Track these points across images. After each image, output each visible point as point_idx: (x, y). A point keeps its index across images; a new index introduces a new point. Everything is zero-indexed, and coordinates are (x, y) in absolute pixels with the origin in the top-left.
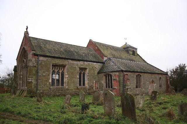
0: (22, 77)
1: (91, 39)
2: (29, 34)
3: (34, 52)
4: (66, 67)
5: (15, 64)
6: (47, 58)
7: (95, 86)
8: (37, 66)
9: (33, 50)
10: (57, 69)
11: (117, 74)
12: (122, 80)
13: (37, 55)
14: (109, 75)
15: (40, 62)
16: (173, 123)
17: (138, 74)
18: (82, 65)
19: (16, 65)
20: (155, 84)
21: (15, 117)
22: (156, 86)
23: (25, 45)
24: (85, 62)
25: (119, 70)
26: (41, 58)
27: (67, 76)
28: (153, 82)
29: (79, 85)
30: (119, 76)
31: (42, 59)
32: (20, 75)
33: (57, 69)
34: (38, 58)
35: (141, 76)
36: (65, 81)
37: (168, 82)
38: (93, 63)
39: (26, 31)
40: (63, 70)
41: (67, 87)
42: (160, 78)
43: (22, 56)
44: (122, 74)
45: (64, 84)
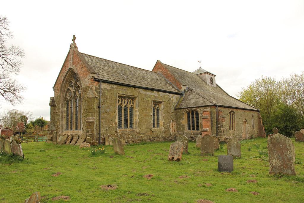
0: (65, 114)
1: (8, 20)
2: (77, 48)
3: (94, 75)
4: (137, 99)
5: (52, 94)
6: (112, 86)
8: (98, 98)
9: (92, 73)
11: (209, 109)
12: (216, 119)
13: (98, 81)
15: (102, 92)
17: (231, 110)
19: (53, 96)
20: (248, 125)
21: (98, 164)
22: (248, 126)
23: (73, 63)
24: (160, 93)
25: (211, 104)
26: (104, 86)
27: (138, 113)
28: (245, 121)
29: (152, 126)
32: (62, 112)
34: (100, 86)
35: (234, 112)
36: (134, 120)
37: (261, 121)
38: (169, 94)
40: (132, 103)
41: (138, 130)
42: (253, 115)
43: (67, 81)
44: (215, 110)
45: (134, 125)
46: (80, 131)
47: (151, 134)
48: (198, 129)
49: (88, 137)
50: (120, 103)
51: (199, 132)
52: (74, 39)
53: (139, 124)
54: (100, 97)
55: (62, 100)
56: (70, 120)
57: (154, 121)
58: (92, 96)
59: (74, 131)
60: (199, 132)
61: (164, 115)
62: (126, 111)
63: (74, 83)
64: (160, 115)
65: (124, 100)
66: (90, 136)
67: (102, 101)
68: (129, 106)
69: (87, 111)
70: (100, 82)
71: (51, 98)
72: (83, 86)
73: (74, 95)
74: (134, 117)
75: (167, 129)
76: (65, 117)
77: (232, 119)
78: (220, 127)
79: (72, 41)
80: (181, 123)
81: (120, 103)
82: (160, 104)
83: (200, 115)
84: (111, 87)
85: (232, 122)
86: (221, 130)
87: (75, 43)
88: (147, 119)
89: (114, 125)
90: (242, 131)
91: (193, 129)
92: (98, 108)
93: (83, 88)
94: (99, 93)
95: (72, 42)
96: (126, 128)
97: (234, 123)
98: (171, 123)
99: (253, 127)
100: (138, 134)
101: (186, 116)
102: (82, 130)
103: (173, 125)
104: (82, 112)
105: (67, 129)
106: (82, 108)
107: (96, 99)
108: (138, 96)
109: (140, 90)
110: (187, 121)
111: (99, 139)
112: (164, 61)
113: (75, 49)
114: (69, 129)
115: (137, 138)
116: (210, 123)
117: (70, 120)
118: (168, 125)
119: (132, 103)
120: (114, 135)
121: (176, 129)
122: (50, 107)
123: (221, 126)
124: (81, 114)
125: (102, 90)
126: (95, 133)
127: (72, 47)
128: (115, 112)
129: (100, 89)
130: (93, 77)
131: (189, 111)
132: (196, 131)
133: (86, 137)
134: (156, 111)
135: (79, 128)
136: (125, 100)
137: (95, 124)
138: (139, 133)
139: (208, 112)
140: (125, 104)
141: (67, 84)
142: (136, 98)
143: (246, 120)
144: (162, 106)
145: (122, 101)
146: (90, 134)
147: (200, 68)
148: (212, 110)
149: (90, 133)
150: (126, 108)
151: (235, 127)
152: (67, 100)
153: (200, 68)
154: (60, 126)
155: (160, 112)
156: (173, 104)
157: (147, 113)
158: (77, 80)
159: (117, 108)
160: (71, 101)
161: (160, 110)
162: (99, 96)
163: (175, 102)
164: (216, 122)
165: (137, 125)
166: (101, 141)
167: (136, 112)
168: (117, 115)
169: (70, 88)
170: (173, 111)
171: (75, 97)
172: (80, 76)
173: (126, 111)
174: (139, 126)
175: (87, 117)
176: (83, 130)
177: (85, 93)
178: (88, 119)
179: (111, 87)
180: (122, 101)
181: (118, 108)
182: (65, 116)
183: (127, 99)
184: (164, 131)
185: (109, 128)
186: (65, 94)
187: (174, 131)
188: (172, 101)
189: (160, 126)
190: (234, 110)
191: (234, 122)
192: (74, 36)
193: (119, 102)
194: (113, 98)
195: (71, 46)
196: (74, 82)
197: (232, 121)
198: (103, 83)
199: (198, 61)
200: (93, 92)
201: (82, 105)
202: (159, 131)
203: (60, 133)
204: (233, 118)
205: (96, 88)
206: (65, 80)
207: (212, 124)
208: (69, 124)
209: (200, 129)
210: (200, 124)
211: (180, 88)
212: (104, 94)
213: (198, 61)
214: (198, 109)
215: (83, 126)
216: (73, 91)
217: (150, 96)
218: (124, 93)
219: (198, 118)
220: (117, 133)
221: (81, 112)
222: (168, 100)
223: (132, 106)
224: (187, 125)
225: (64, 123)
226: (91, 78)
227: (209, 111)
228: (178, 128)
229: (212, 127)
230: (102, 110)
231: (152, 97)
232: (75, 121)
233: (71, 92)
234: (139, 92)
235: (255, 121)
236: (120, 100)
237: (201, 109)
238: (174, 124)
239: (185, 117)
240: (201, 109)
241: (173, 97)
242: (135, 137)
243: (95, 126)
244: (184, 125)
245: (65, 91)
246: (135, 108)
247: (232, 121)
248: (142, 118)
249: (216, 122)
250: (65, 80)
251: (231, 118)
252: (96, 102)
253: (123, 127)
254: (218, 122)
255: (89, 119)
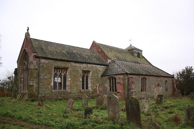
0: (22, 80)
2: (30, 36)
3: (35, 54)
4: (69, 69)
5: (16, 66)
6: (49, 61)
7: (99, 90)
8: (38, 69)
9: (34, 53)
10: (59, 72)
11: (122, 76)
12: (127, 83)
13: (38, 57)
14: (113, 78)
15: (41, 65)
16: (179, 128)
17: (143, 77)
18: (85, 68)
19: (17, 67)
20: (161, 88)
22: (162, 89)
23: (26, 47)
24: (89, 65)
25: (124, 73)
26: (43, 61)
27: (70, 79)
28: (158, 85)
29: (81, 89)
30: (123, 79)
31: (43, 62)
32: (21, 78)
33: (59, 72)
34: (39, 61)
35: (146, 79)
36: (67, 84)
37: (174, 85)
38: (96, 66)
39: (27, 32)
40: (65, 72)
41: (69, 91)
42: (166, 81)
43: (23, 58)
44: (126, 77)
45: (67, 88)
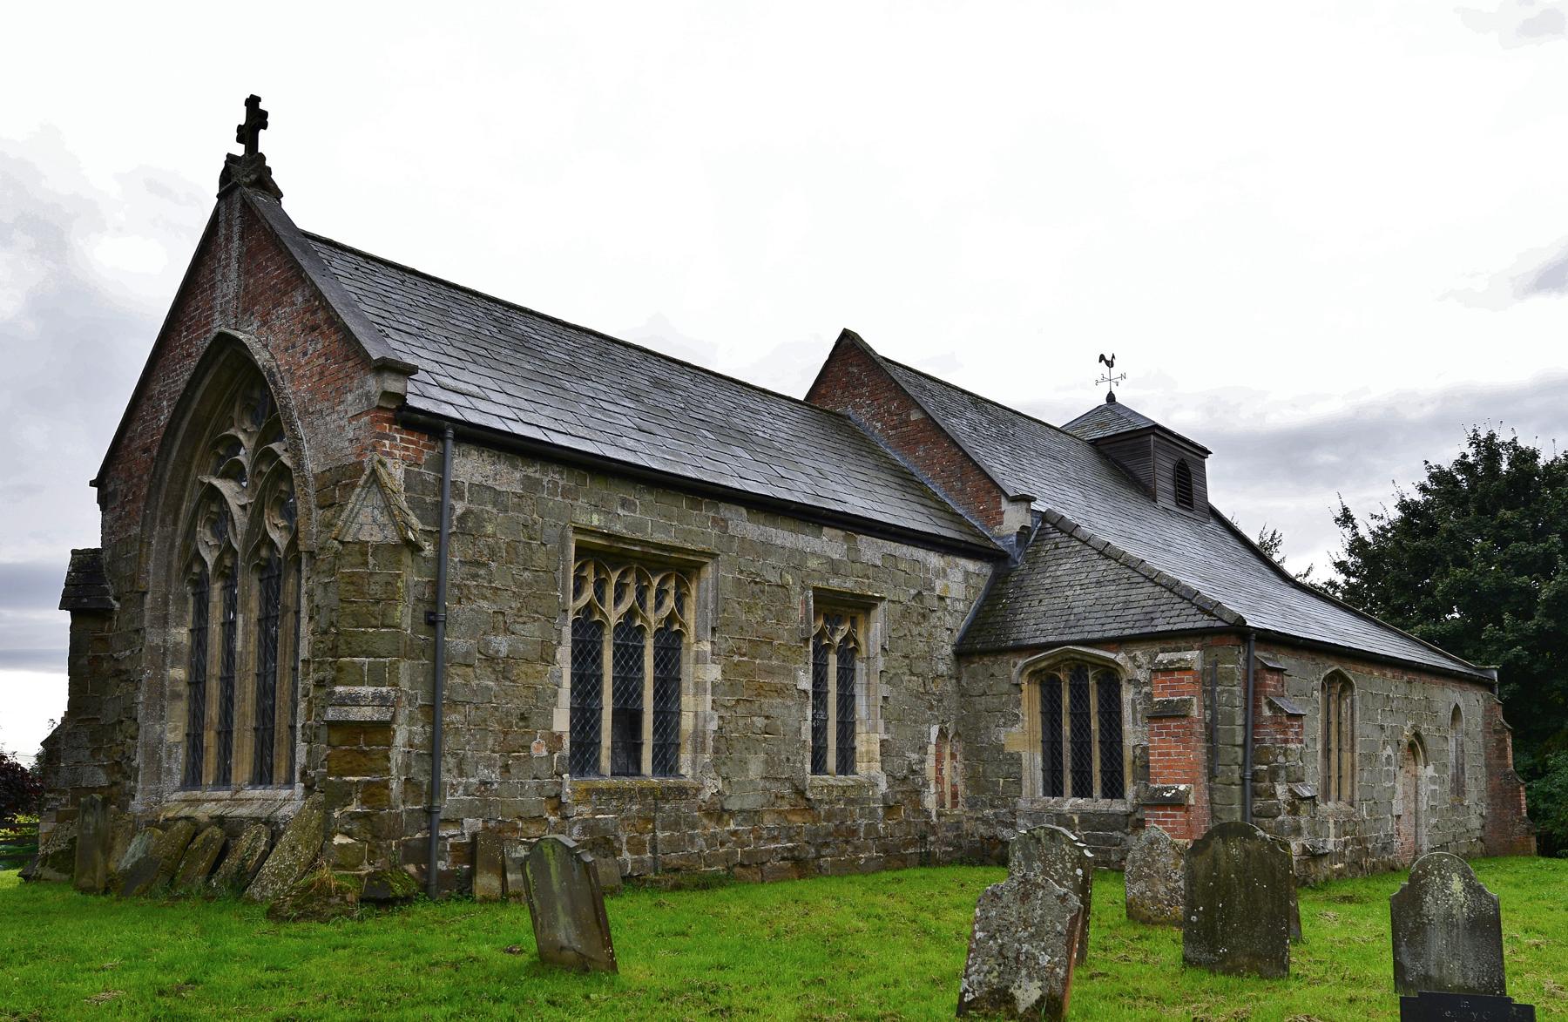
0: (179, 673)
2: (278, 195)
4: (708, 572)
6: (533, 472)
7: (939, 780)
8: (428, 549)
10: (618, 599)
11: (1192, 656)
14: (1079, 667)
15: (460, 508)
16: (950, 1021)
18: (834, 567)
20: (1430, 771)
22: (1432, 780)
25: (1202, 622)
26: (468, 467)
28: (1416, 747)
29: (808, 767)
30: (1210, 680)
31: (477, 479)
33: (618, 599)
34: (441, 465)
35: (1347, 685)
36: (687, 723)
38: (919, 553)
39: (239, 150)
40: (670, 603)
41: (712, 786)
44: (1234, 664)
45: (685, 757)
46: (285, 793)
47: (797, 820)
48: (1114, 789)
49: (339, 840)
50: (589, 594)
51: (1118, 807)
52: (255, 118)
53: (716, 751)
54: (439, 547)
55: (163, 573)
56: (213, 711)
57: (819, 731)
58: (377, 537)
59: (241, 795)
60: (1118, 807)
61: (885, 690)
62: (628, 658)
63: (253, 443)
64: (860, 691)
65: (615, 577)
66: (355, 827)
67: (455, 571)
68: (653, 619)
69: (333, 647)
70: (443, 440)
71: (74, 552)
72: (312, 466)
73: (250, 533)
74: (687, 701)
75: (908, 784)
76: (176, 696)
77: (1333, 729)
78: (1273, 780)
79: (239, 140)
80: (1000, 748)
81: (589, 594)
82: (861, 618)
83: (1128, 695)
84: (526, 476)
85: (1334, 745)
86: (1274, 795)
87: (262, 157)
88: (773, 713)
89: (539, 749)
90: (1398, 808)
91: (1082, 789)
92: (423, 627)
93: (315, 477)
94: (438, 512)
95: (239, 150)
96: (627, 775)
97: (1346, 756)
98: (932, 749)
99: (1459, 789)
100: (709, 814)
101: (1030, 702)
102: (299, 787)
103: (947, 764)
104: (304, 653)
105: (193, 778)
106: (304, 620)
107: (406, 558)
108: (713, 556)
109: (727, 511)
110: (1040, 736)
111: (424, 853)
112: (883, 345)
113: (261, 199)
114: (243, 767)
115: (701, 842)
116: (1197, 753)
117: (213, 711)
118: (914, 756)
119: (670, 603)
120: (539, 819)
121: (961, 788)
122: (69, 621)
123: (1273, 775)
124: (295, 669)
125: (461, 498)
126: (401, 804)
127: (236, 186)
128: (548, 657)
129: (442, 491)
130: (386, 395)
131: (1055, 667)
132: (1098, 804)
133: (329, 836)
134: (833, 660)
135: (281, 772)
136: (623, 575)
137: (400, 736)
138: (717, 813)
139: (1187, 677)
140: (623, 608)
141: (197, 457)
142: (699, 566)
143: (1417, 735)
144: (875, 631)
145: (600, 587)
146: (354, 817)
147: (1111, 398)
148: (1216, 663)
149: (354, 807)
150: (629, 632)
151: (1357, 779)
152: (196, 569)
153: (1111, 398)
154: (138, 760)
155: (860, 666)
156: (949, 621)
157: (770, 671)
158: (273, 425)
159: (567, 632)
160: (228, 576)
161: (858, 656)
162: (438, 537)
163: (960, 606)
164: (1244, 746)
165: (704, 750)
166: (442, 865)
167: (697, 661)
168: (567, 683)
169: (226, 487)
170: (942, 668)
171: (257, 549)
172: (293, 393)
173: (628, 658)
174: (716, 765)
175: (339, 689)
176: (309, 789)
177: (329, 513)
178: (343, 702)
179: (526, 476)
180: (600, 587)
181: (575, 632)
182: (183, 689)
183: (640, 577)
184: (885, 796)
185: (506, 768)
186: (182, 526)
187: (948, 798)
188: (941, 598)
189: (861, 767)
190: (1351, 672)
191: (1346, 747)
192: (252, 102)
193: (578, 592)
194: (540, 560)
195: (225, 177)
196: (248, 443)
197: (1336, 739)
198: (464, 447)
199: (1102, 358)
200: (388, 508)
201: (304, 601)
202: (850, 802)
203: (137, 805)
204: (1340, 724)
205: (410, 481)
206: (185, 424)
207: (1212, 753)
208: (210, 738)
209: (1130, 791)
210: (1128, 755)
211: (997, 517)
212: (469, 527)
213: (1102, 358)
214: (1120, 658)
215: (309, 753)
216: (243, 507)
217: (796, 559)
218: (618, 528)
219: (1119, 713)
220: (558, 804)
221: (296, 653)
222: (913, 592)
223: (670, 619)
224: (1039, 759)
225: (171, 737)
226: (376, 401)
227: (1197, 666)
228: (976, 782)
229: (1212, 775)
230: (457, 642)
231: (813, 563)
232: (251, 723)
233: (226, 514)
234: (721, 524)
235: (1471, 748)
236: (592, 579)
237: (1138, 653)
238: (953, 756)
239: (1025, 703)
240: (1138, 653)
241: (945, 575)
242: (692, 837)
243: (397, 757)
244: (1016, 760)
245: (186, 506)
246: (690, 637)
247: (1336, 739)
248: (741, 710)
249: (1239, 740)
250: (185, 424)
251: (1329, 723)
252: (412, 577)
253: (606, 763)
254: (1253, 749)
255: (355, 701)
